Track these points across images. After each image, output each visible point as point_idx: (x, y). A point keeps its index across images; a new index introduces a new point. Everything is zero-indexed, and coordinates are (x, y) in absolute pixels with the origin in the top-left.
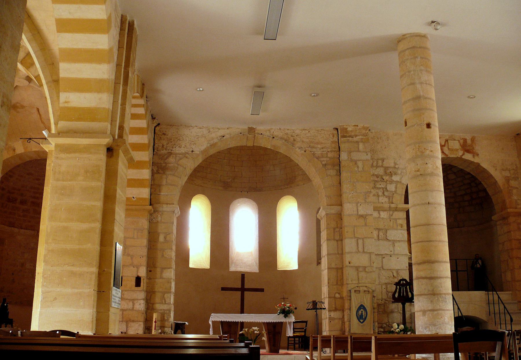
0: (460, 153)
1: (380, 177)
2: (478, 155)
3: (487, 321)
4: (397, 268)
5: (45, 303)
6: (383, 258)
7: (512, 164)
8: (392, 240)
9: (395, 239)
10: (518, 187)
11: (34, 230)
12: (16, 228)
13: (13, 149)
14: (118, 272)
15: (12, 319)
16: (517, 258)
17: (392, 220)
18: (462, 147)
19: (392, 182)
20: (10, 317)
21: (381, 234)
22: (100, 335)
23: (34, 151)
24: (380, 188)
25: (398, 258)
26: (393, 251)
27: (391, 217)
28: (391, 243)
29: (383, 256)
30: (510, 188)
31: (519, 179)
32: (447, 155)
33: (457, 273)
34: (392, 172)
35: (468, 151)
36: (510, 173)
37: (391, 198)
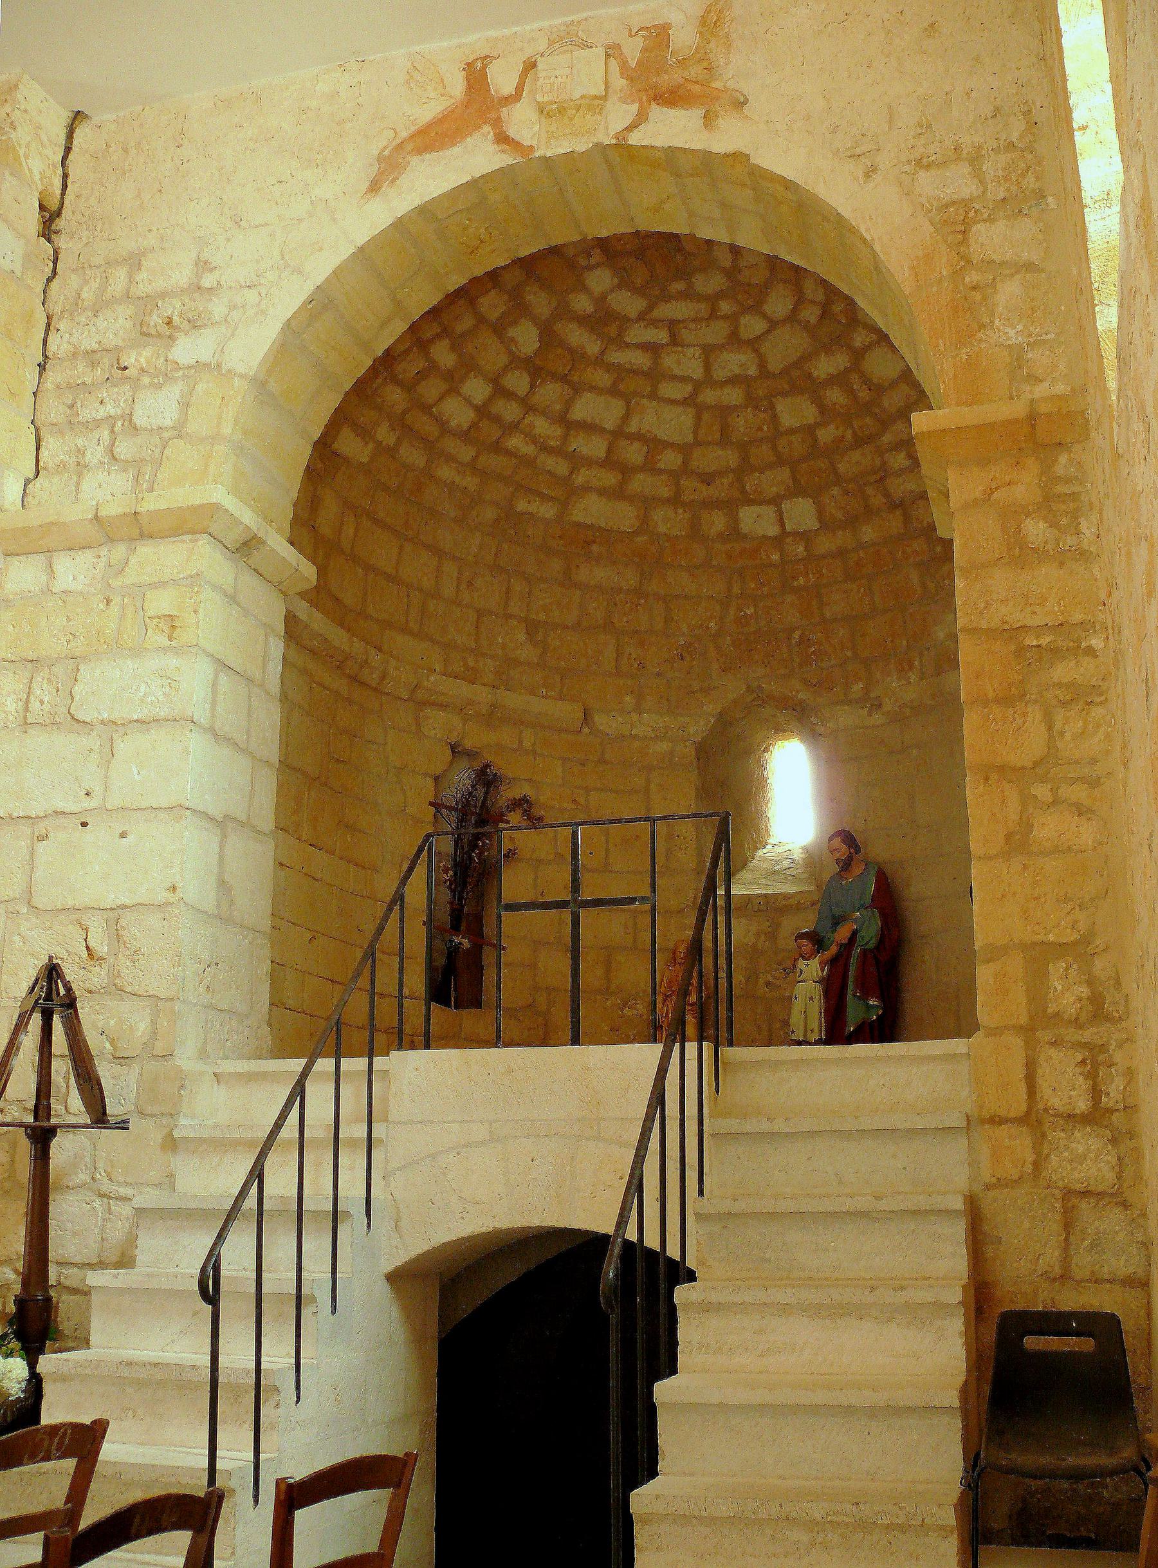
0: (619, 115)
1: (106, 360)
2: (740, 104)
4: (110, 900)
6: (42, 838)
7: (997, 112)
8: (103, 722)
9: (120, 713)
10: (1036, 259)
16: (994, 777)
17: (116, 600)
18: (631, 79)
19: (163, 376)
21: (43, 690)
22: (730, 1008)
24: (98, 423)
25: (123, 835)
26: (97, 789)
27: (117, 583)
28: (92, 741)
29: (41, 828)
30: (972, 277)
31: (1050, 199)
32: (531, 148)
33: (561, 905)
34: (176, 319)
35: (672, 97)
36: (978, 175)
37: (148, 470)
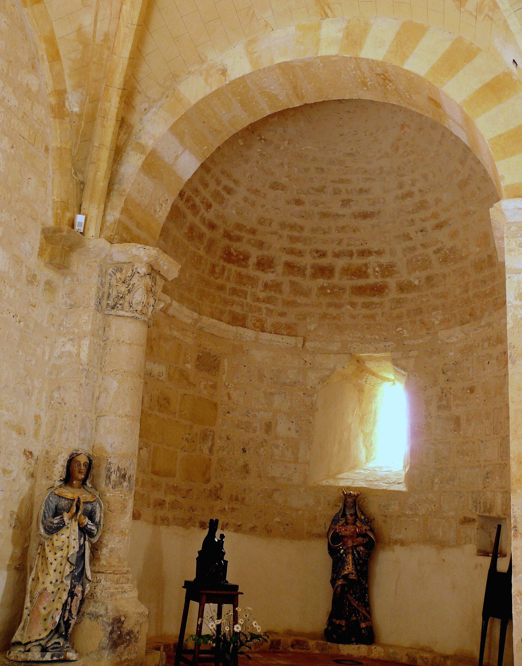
3: (503, 516)
5: (92, 92)
11: (296, 336)
12: (248, 328)
13: (220, 69)
14: (38, 588)
15: (236, 587)
20: (231, 578)
23: (279, 65)
